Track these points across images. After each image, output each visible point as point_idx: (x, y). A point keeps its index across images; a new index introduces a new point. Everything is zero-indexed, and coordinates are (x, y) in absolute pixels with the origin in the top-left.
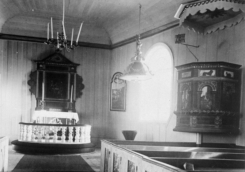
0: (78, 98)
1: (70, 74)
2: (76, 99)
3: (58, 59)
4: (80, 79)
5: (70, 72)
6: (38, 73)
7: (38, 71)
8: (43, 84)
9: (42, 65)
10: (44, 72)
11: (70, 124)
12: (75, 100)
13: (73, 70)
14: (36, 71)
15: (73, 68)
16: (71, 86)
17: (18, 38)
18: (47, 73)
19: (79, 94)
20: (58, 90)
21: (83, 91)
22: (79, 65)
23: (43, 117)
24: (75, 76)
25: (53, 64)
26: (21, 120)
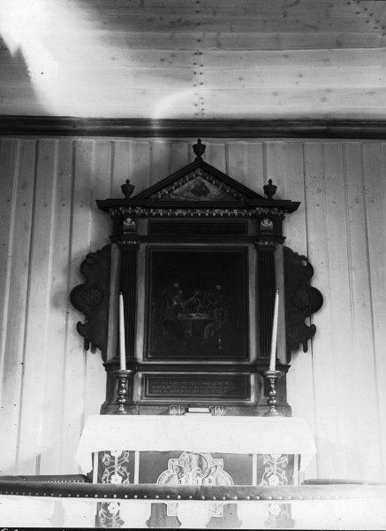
0: (296, 349)
1: (256, 246)
2: (289, 359)
3: (199, 190)
4: (301, 270)
5: (254, 240)
6: (115, 254)
7: (114, 246)
8: (277, 296)
9: (134, 219)
10: (143, 246)
11: (116, 480)
12: (283, 361)
13: (267, 230)
14: (107, 249)
15: (267, 224)
16: (119, 298)
17: (374, 128)
18: (156, 257)
19: (300, 337)
20: (206, 322)
21: (318, 320)
22: (292, 207)
23: (93, 454)
24: (279, 256)
25: (180, 216)
26: (38, 466)
